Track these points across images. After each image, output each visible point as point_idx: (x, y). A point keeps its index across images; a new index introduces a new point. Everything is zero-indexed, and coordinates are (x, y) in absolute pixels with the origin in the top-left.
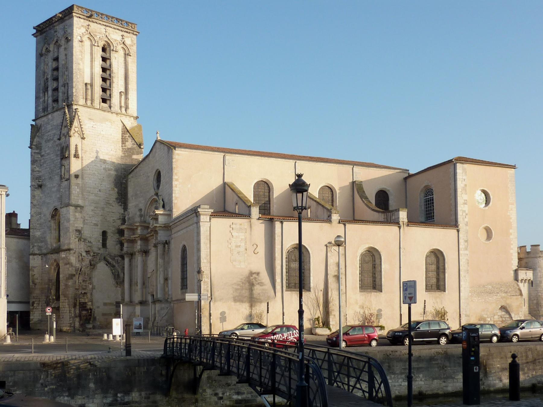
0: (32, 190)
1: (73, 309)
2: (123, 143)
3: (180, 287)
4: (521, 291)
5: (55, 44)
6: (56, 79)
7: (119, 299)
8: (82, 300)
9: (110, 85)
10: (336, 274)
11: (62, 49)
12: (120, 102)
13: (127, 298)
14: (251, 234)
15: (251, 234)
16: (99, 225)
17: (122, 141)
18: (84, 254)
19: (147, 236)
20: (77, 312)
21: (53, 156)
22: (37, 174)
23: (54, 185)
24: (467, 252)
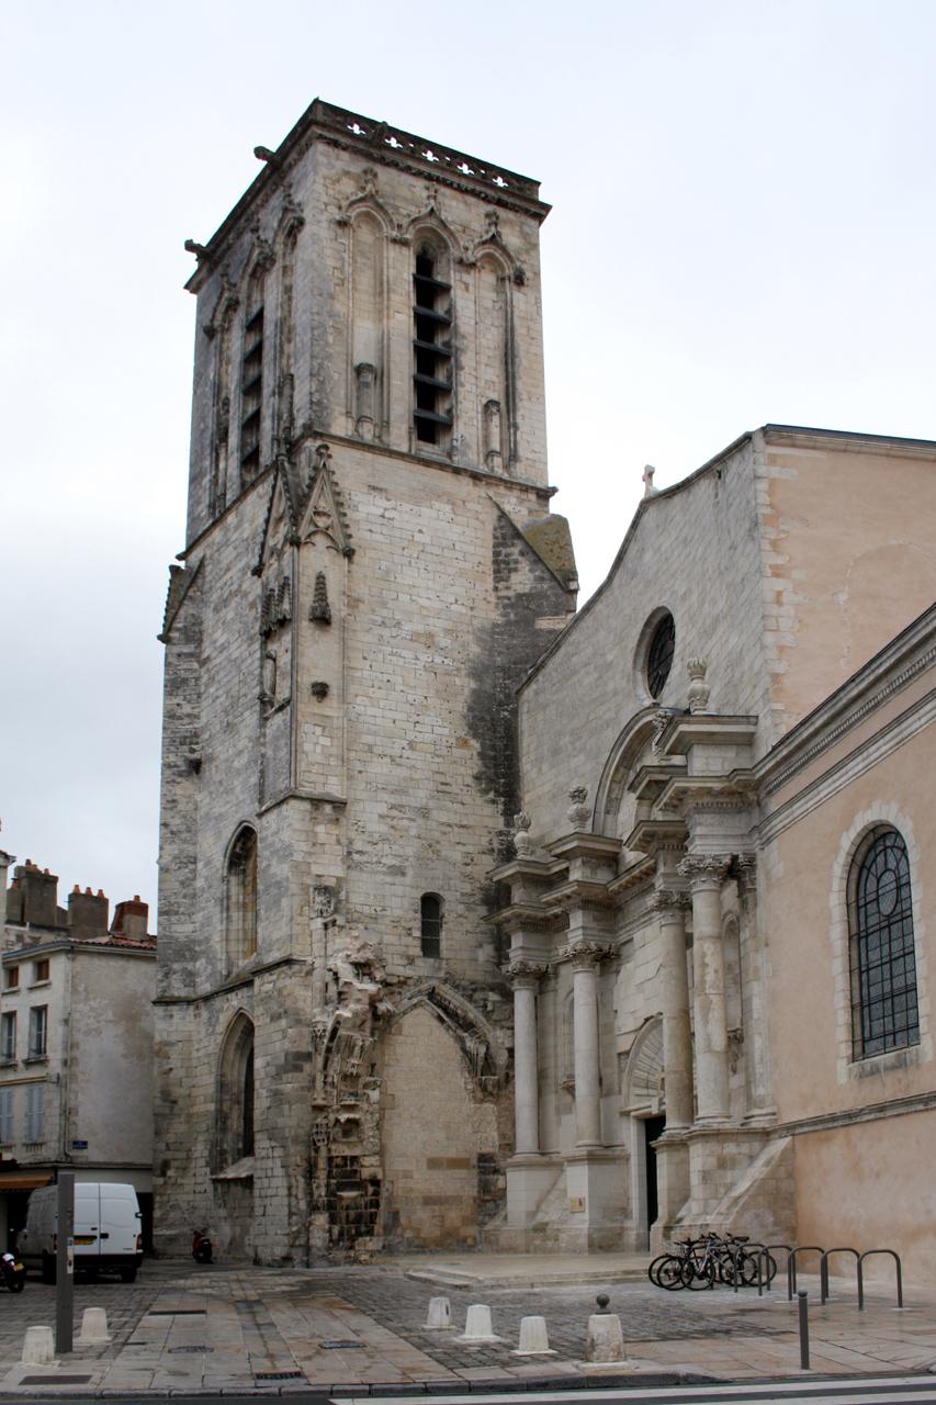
2: (497, 580)
3: (845, 1050)
9: (449, 377)
16: (410, 872)
17: (497, 571)
18: (347, 974)
20: (321, 1192)
21: (236, 650)
22: (185, 727)
23: (240, 746)
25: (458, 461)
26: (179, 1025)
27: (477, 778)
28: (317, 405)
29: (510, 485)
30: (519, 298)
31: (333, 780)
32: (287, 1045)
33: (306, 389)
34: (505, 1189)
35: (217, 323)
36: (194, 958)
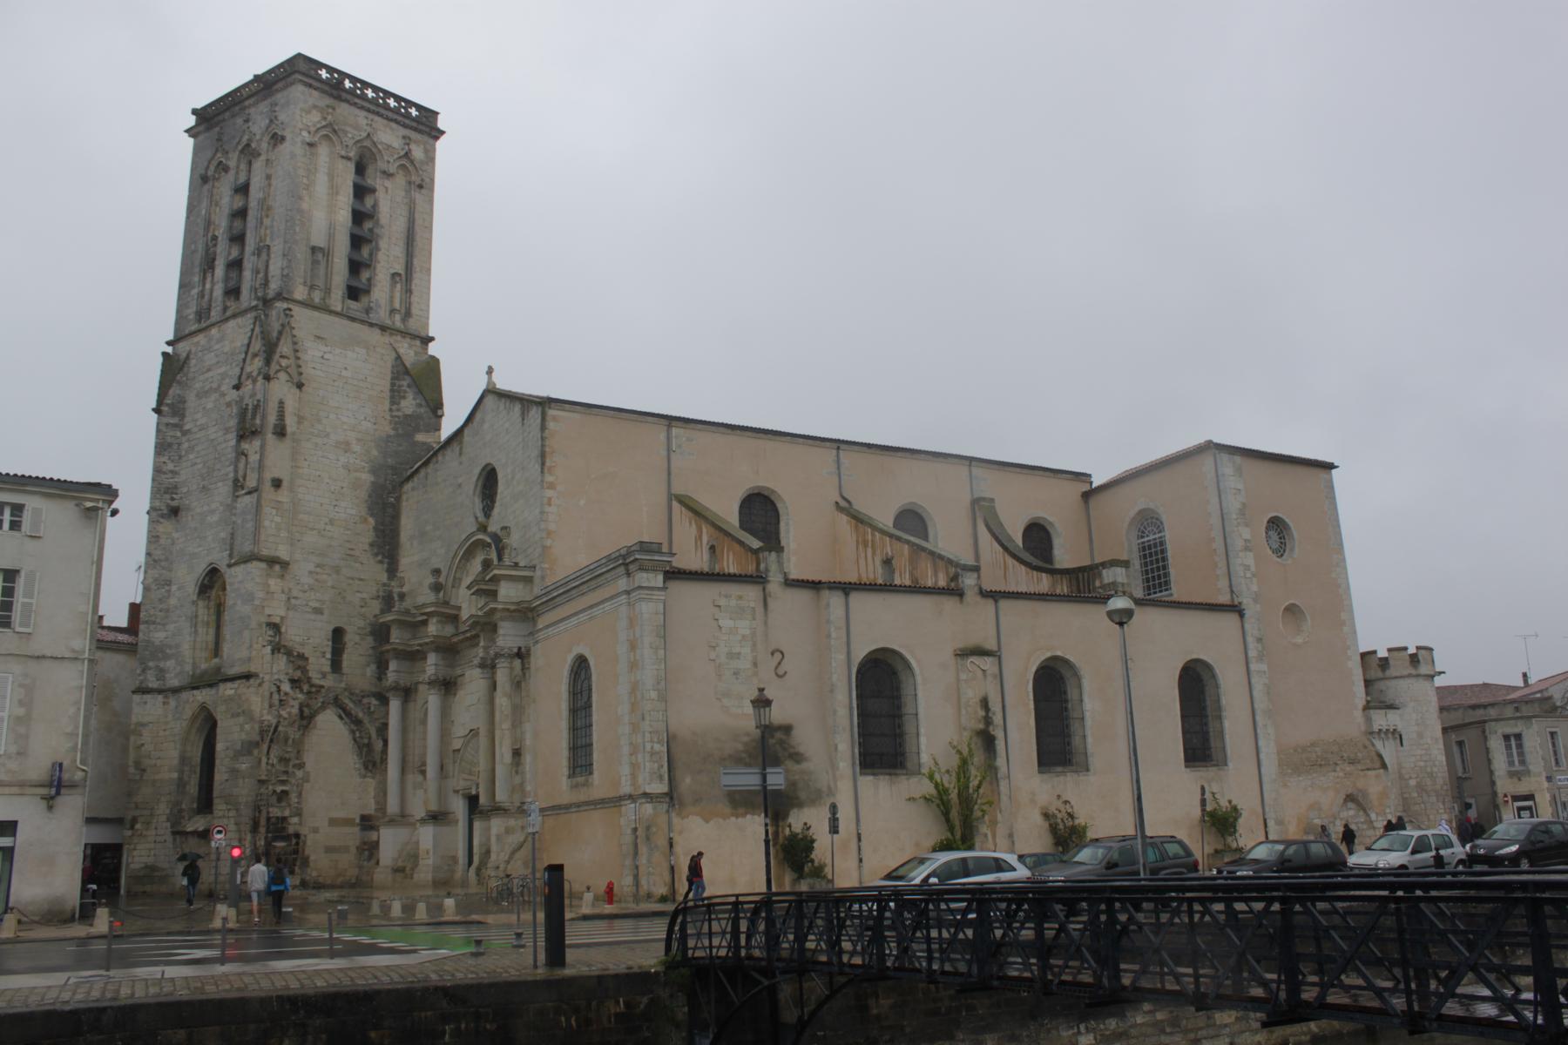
0: (151, 522)
1: (249, 837)
2: (393, 403)
3: (565, 771)
4: (1380, 756)
5: (242, 152)
6: (238, 239)
7: (371, 809)
8: (276, 812)
10: (981, 726)
11: (258, 165)
12: (392, 298)
13: (393, 806)
14: (766, 623)
15: (766, 623)
16: (326, 612)
17: (392, 397)
18: (286, 687)
19: (455, 640)
23: (213, 506)
24: (1264, 667)
25: (373, 318)
26: (149, 710)
27: (371, 545)
28: (286, 277)
29: (404, 334)
30: (419, 197)
31: (281, 547)
32: (244, 736)
33: (279, 264)
34: (377, 842)
35: (210, 173)
36: (166, 657)
